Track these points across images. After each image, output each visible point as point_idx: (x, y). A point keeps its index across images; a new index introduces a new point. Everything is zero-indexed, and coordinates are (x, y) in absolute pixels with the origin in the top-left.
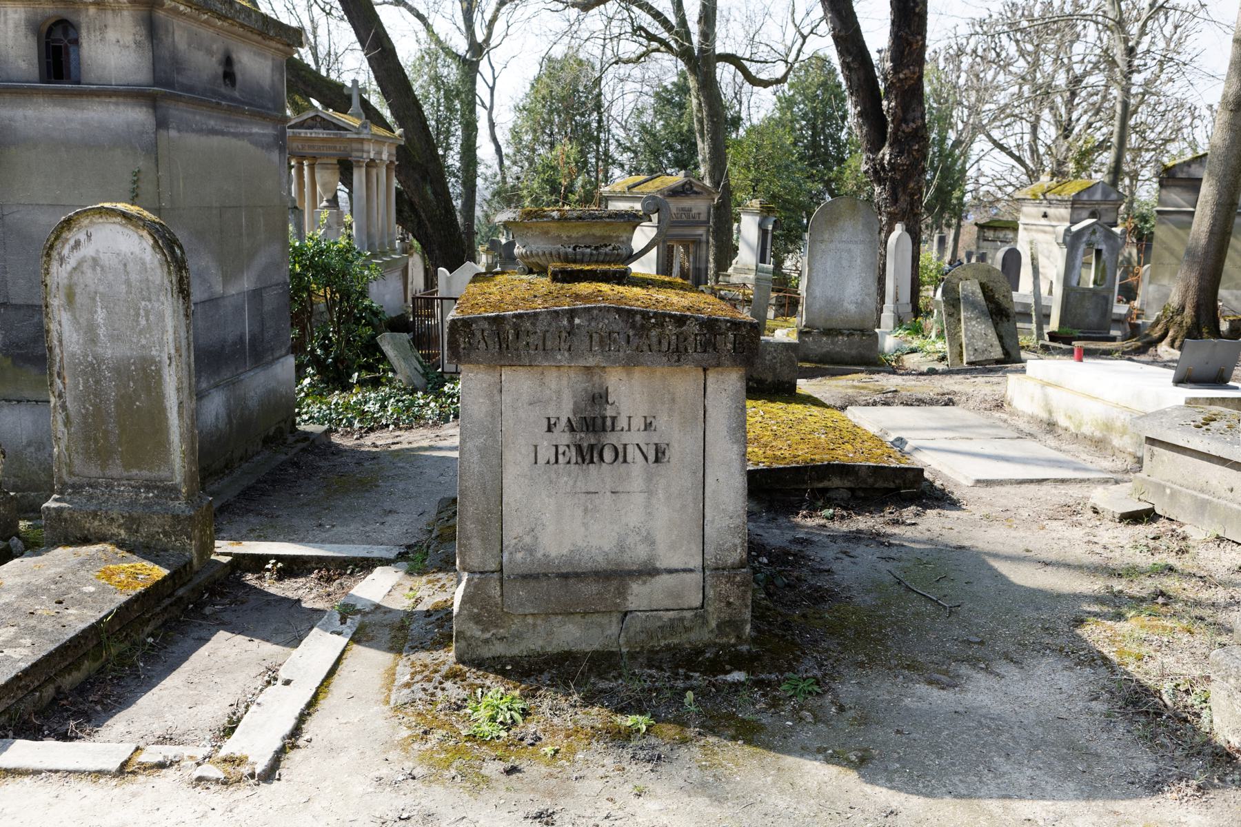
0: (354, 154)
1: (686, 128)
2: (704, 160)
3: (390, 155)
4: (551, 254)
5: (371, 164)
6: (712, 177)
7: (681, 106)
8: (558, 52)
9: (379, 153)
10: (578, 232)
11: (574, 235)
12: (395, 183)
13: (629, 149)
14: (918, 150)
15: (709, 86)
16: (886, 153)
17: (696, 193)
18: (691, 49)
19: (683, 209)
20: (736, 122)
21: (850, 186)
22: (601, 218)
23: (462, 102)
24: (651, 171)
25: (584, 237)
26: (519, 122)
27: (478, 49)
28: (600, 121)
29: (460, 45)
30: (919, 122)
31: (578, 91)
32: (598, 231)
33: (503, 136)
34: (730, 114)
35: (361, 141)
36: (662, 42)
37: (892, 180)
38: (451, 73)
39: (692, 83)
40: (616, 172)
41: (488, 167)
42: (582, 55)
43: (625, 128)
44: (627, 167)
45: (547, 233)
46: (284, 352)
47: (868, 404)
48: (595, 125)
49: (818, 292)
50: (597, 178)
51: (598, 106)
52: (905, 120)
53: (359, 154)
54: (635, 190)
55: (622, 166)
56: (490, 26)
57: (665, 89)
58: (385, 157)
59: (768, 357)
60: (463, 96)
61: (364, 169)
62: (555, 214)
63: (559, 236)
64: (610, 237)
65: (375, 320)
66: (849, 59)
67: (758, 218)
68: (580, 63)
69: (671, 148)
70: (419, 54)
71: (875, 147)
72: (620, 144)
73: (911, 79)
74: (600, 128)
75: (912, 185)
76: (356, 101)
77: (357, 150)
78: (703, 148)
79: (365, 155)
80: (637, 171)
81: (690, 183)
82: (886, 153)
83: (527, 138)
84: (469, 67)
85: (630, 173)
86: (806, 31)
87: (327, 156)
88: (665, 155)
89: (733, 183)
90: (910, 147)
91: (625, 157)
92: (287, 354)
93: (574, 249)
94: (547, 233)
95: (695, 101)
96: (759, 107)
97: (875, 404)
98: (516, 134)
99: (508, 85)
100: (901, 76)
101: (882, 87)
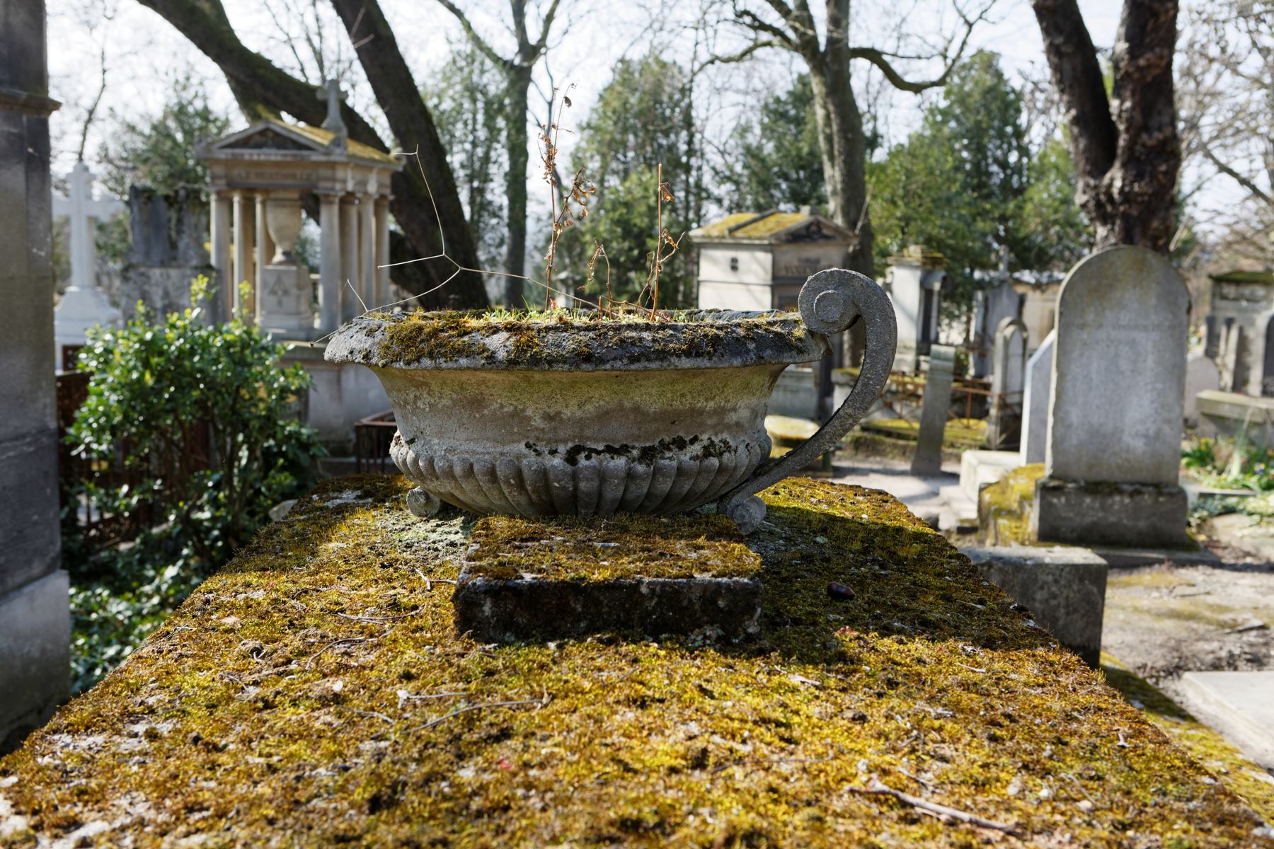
0: (323, 184)
1: (806, 150)
2: (834, 193)
3: (381, 186)
4: (492, 473)
5: (347, 200)
6: (846, 214)
7: (799, 122)
8: (636, 54)
9: (363, 183)
10: (582, 402)
11: (570, 411)
12: (392, 224)
13: (729, 179)
14: (1166, 173)
15: (839, 89)
16: (1116, 178)
17: (827, 237)
18: (814, 40)
19: (808, 260)
20: (873, 142)
21: (1032, 226)
22: (663, 355)
23: (507, 118)
24: (759, 207)
25: (603, 416)
26: (583, 144)
27: (530, 52)
28: (690, 143)
29: (507, 47)
30: (1168, 131)
31: (661, 103)
32: (651, 396)
33: (563, 163)
34: (867, 129)
35: (332, 165)
36: (776, 32)
37: (1126, 217)
38: (495, 82)
39: (817, 86)
40: (711, 209)
41: (542, 203)
42: (667, 57)
43: (723, 153)
44: (726, 203)
45: (477, 403)
46: (37, 568)
47: (1216, 666)
48: (683, 147)
49: (1075, 416)
50: (686, 218)
51: (688, 123)
52: (1146, 128)
53: (328, 185)
54: (739, 234)
55: (719, 201)
56: (549, 18)
57: (778, 100)
58: (372, 188)
59: (1039, 596)
60: (509, 112)
61: (336, 208)
62: (499, 343)
63: (518, 415)
64: (695, 413)
65: (304, 459)
66: (1059, 40)
67: (918, 274)
68: (664, 65)
69: (786, 177)
70: (450, 58)
71: (1098, 166)
72: (717, 173)
73: (1158, 66)
74: (691, 152)
75: (1155, 224)
76: (334, 109)
77: (326, 179)
78: (833, 174)
79: (338, 186)
80: (738, 207)
81: (818, 224)
82: (1116, 178)
83: (594, 165)
84: (519, 77)
85: (730, 210)
86: (971, 18)
87: (286, 188)
88: (777, 186)
89: (875, 223)
90: (1154, 167)
91: (724, 190)
92: (49, 571)
93: (571, 458)
94: (477, 403)
95: (820, 113)
96: (897, 120)
97: (1231, 663)
98: (578, 163)
99: (570, 94)
100: (1142, 62)
101: (1109, 85)
